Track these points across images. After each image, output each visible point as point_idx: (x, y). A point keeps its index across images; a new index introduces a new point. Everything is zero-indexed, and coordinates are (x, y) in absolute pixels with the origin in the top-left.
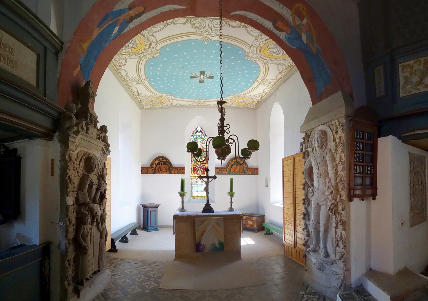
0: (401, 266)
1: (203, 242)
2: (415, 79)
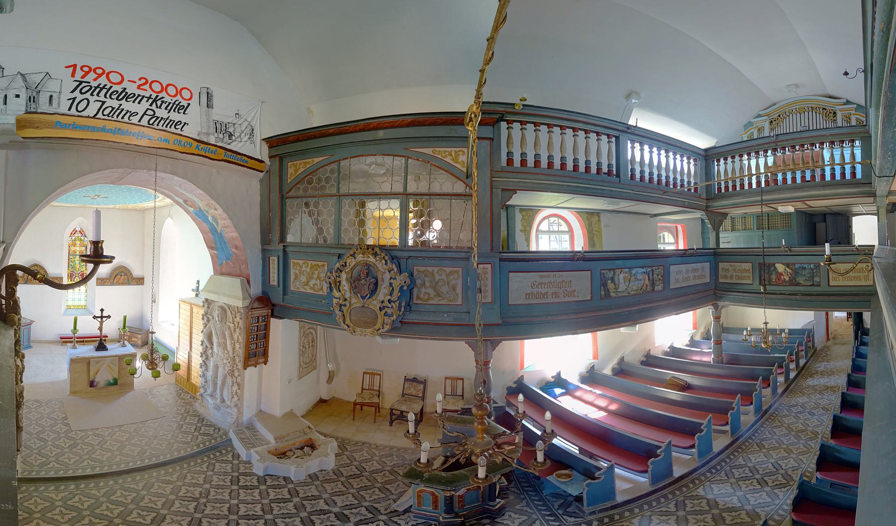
0: (287, 410)
1: (97, 380)
2: (303, 279)
